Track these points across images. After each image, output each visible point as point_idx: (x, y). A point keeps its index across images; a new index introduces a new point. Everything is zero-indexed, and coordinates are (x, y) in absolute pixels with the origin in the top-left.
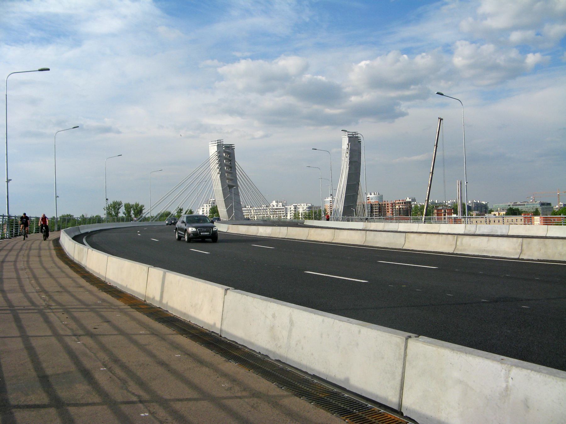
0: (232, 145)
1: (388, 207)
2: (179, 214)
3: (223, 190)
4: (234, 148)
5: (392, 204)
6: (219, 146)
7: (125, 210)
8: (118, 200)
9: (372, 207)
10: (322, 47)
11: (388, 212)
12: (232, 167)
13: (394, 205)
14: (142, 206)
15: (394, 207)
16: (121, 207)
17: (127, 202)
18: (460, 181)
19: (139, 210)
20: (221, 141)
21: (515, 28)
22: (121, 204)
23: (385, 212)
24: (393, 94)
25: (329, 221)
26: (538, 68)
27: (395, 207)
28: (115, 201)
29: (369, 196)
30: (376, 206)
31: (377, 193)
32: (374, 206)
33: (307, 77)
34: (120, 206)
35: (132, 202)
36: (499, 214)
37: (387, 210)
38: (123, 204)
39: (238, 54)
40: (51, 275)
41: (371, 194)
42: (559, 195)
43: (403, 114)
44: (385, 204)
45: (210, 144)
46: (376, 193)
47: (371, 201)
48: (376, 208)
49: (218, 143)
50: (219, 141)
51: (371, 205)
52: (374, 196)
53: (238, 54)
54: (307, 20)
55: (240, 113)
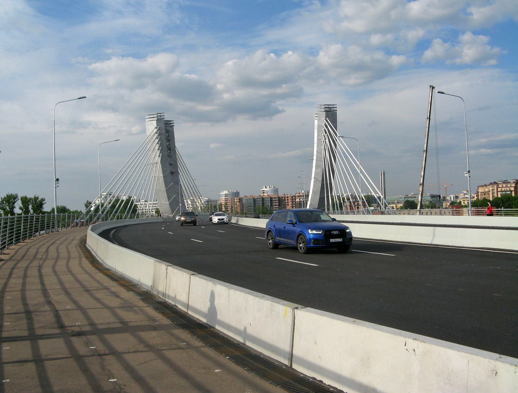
1: (288, 200)
3: (165, 177)
4: (174, 126)
5: (292, 197)
6: (159, 121)
7: (22, 204)
8: (12, 191)
10: (190, 48)
11: (288, 205)
12: (171, 149)
13: (294, 198)
14: (43, 200)
15: (294, 200)
16: (16, 201)
17: (23, 195)
18: (383, 171)
19: (38, 204)
20: (161, 114)
21: (375, 31)
22: (17, 197)
23: (285, 205)
24: (265, 92)
26: (403, 68)
27: (295, 200)
28: (10, 194)
29: (264, 189)
30: (276, 199)
31: (273, 186)
33: (177, 74)
34: (16, 200)
35: (30, 195)
36: (396, 206)
38: (20, 198)
39: (109, 51)
41: (266, 188)
42: (446, 187)
43: (277, 112)
44: (285, 197)
45: (147, 118)
46: (271, 186)
48: (276, 202)
49: (157, 117)
50: (158, 115)
51: (271, 198)
52: (270, 189)
53: (109, 51)
54: (178, 22)
55: (114, 109)
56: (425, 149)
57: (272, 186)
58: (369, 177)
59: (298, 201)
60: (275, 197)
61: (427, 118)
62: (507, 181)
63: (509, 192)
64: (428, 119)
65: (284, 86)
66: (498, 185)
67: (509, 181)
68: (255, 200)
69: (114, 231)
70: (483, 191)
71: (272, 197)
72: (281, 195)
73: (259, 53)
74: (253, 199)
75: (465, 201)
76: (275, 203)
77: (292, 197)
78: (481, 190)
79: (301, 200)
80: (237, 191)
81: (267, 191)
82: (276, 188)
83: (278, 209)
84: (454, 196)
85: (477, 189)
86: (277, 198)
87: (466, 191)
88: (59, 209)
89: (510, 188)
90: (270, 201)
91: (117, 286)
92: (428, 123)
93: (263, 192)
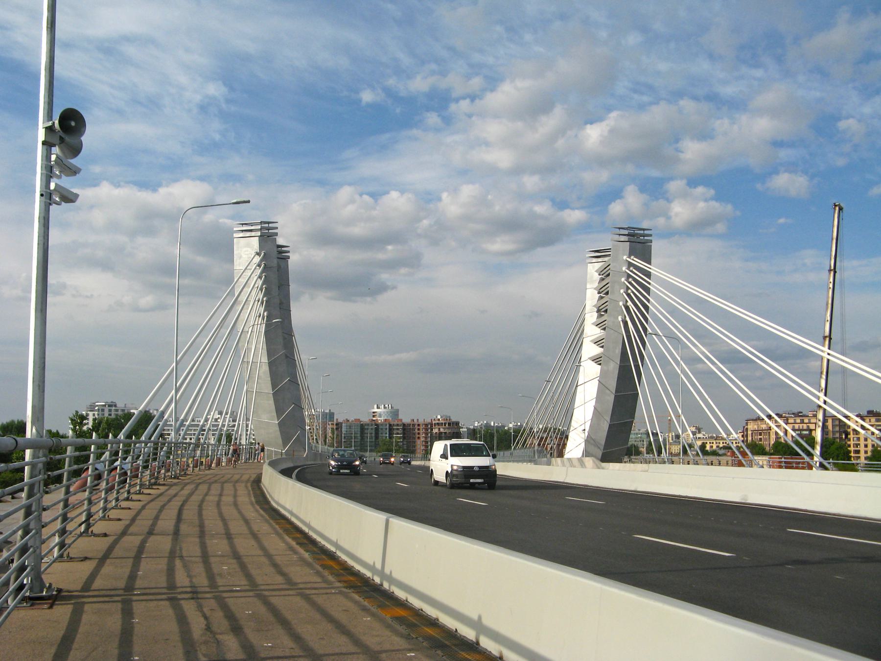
0: (271, 225)
1: (419, 429)
2: (78, 427)
4: (276, 234)
5: (426, 425)
9: (377, 430)
11: (419, 438)
13: (429, 426)
15: (429, 430)
23: (414, 438)
24: (359, 256)
25: (550, 465)
27: (432, 430)
29: (376, 410)
31: (390, 406)
32: (395, 427)
37: (417, 436)
40: (255, 536)
41: (378, 408)
42: (670, 420)
43: (382, 288)
44: (414, 425)
46: (387, 406)
47: (379, 419)
51: (390, 425)
52: (385, 410)
56: (827, 333)
57: (388, 405)
58: (698, 382)
59: (436, 433)
60: (398, 424)
61: (830, 270)
62: (802, 413)
63: (807, 432)
64: (832, 273)
65: (390, 247)
66: (787, 420)
67: (804, 413)
68: (363, 427)
69: (299, 469)
70: (756, 427)
71: (392, 423)
72: (406, 420)
73: (345, 192)
74: (359, 425)
75: (713, 443)
76: (398, 434)
77: (426, 424)
78: (751, 426)
79: (442, 430)
80: (330, 410)
81: (381, 413)
82: (395, 408)
83: (402, 444)
84: (674, 434)
85: (744, 425)
86: (400, 426)
87: (694, 428)
88: (14, 427)
89: (808, 424)
90: (388, 430)
91: (357, 653)
92: (831, 280)
93: (374, 414)
